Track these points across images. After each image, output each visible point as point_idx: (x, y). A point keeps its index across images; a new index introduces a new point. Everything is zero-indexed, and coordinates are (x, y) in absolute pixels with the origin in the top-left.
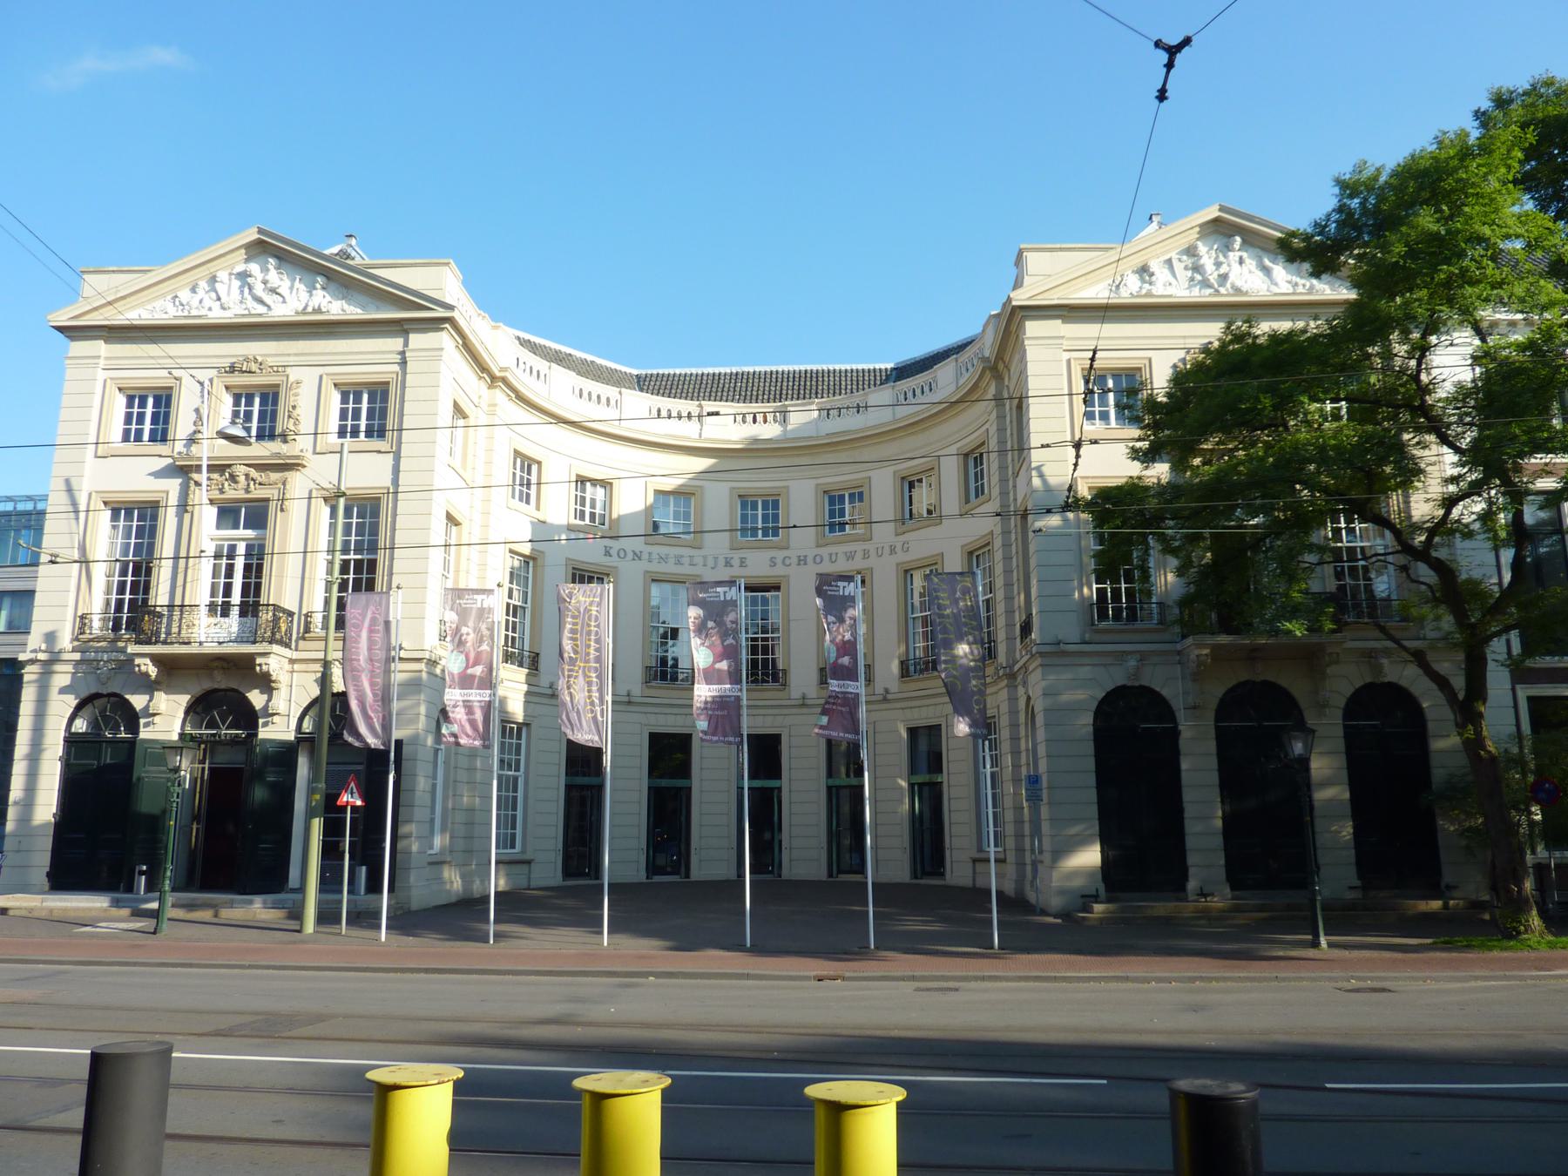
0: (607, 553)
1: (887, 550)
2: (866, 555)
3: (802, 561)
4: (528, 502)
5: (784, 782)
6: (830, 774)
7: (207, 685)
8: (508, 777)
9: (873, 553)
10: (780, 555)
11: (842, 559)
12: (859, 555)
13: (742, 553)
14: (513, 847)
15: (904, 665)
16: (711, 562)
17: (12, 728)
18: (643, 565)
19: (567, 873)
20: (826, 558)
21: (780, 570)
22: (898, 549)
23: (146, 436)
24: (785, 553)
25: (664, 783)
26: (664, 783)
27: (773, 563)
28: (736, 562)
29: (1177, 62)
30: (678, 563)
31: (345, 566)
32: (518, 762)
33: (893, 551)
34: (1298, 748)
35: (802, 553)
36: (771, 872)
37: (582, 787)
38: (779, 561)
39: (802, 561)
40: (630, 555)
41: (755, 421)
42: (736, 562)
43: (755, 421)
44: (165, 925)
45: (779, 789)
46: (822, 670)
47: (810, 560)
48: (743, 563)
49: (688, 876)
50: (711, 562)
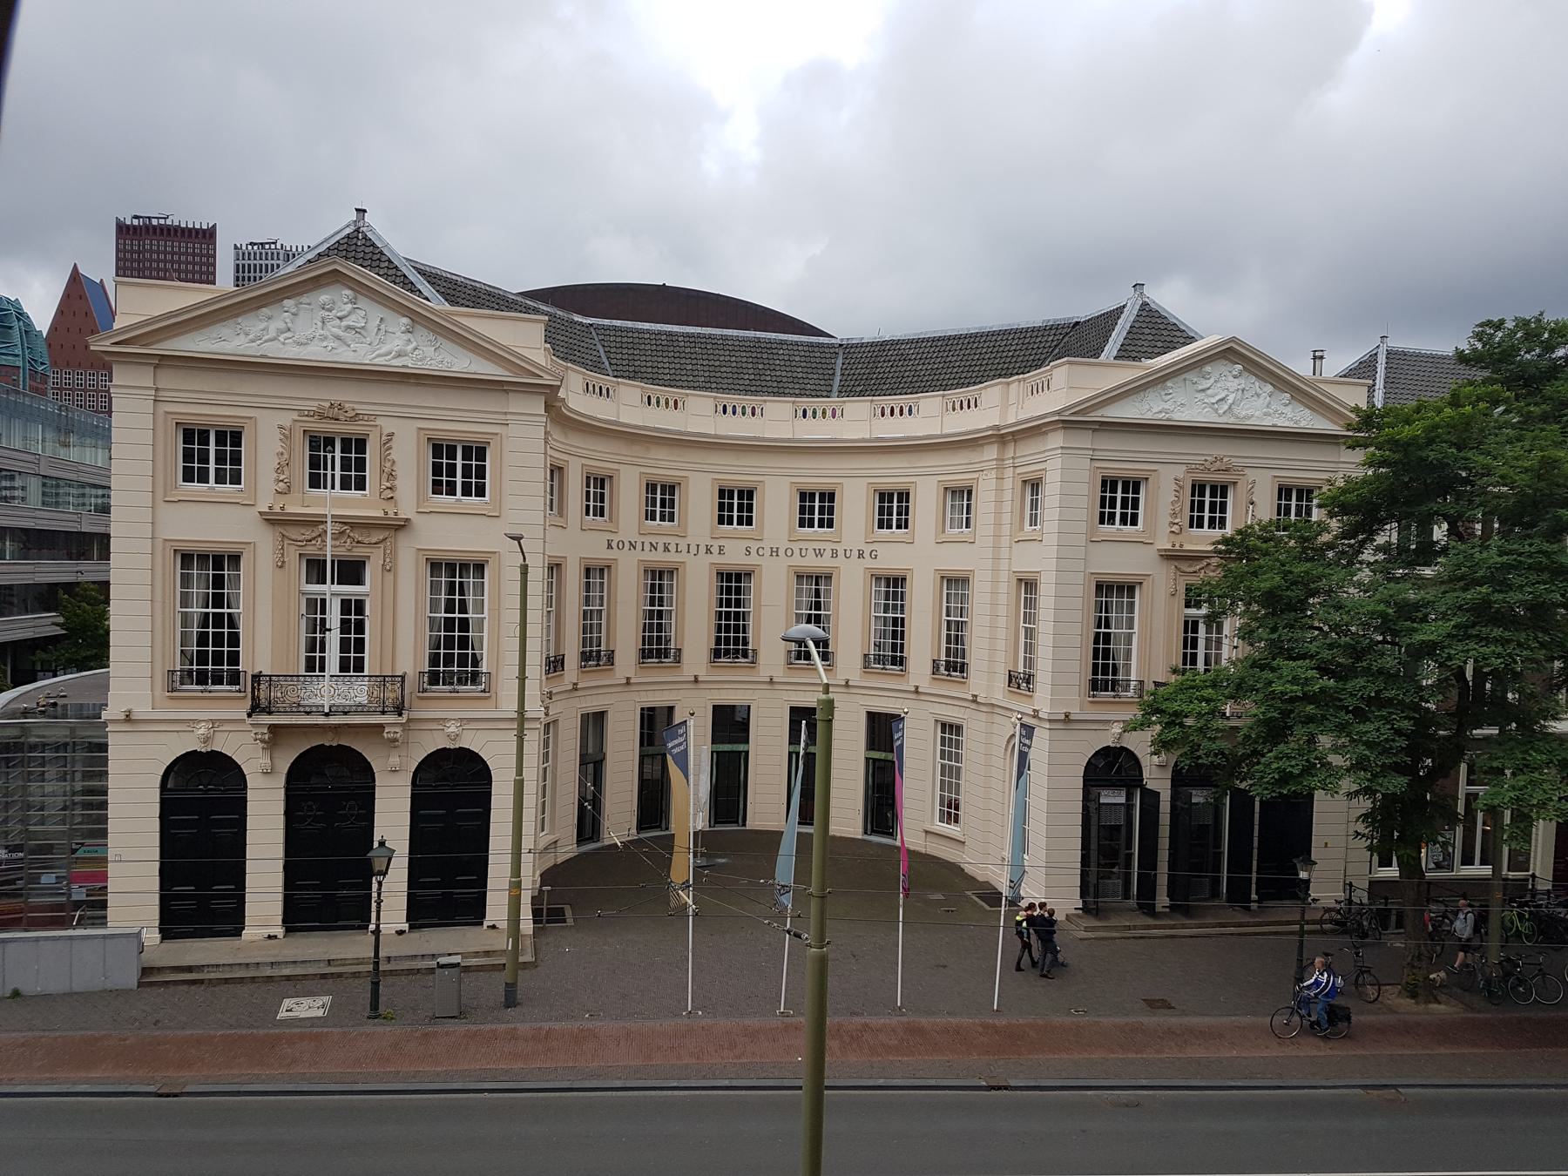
2: (835, 554)
3: (774, 552)
4: (602, 515)
9: (840, 553)
10: (754, 546)
12: (828, 553)
13: (721, 542)
16: (693, 550)
18: (638, 555)
19: (640, 828)
20: (797, 552)
21: (753, 560)
22: (866, 555)
23: (333, 665)
24: (759, 544)
28: (715, 550)
30: (666, 549)
31: (202, 639)
33: (861, 555)
34: (1303, 875)
38: (753, 551)
39: (774, 552)
40: (627, 545)
41: (892, 413)
42: (715, 550)
43: (892, 413)
44: (1298, 917)
45: (747, 753)
47: (781, 552)
50: (693, 550)
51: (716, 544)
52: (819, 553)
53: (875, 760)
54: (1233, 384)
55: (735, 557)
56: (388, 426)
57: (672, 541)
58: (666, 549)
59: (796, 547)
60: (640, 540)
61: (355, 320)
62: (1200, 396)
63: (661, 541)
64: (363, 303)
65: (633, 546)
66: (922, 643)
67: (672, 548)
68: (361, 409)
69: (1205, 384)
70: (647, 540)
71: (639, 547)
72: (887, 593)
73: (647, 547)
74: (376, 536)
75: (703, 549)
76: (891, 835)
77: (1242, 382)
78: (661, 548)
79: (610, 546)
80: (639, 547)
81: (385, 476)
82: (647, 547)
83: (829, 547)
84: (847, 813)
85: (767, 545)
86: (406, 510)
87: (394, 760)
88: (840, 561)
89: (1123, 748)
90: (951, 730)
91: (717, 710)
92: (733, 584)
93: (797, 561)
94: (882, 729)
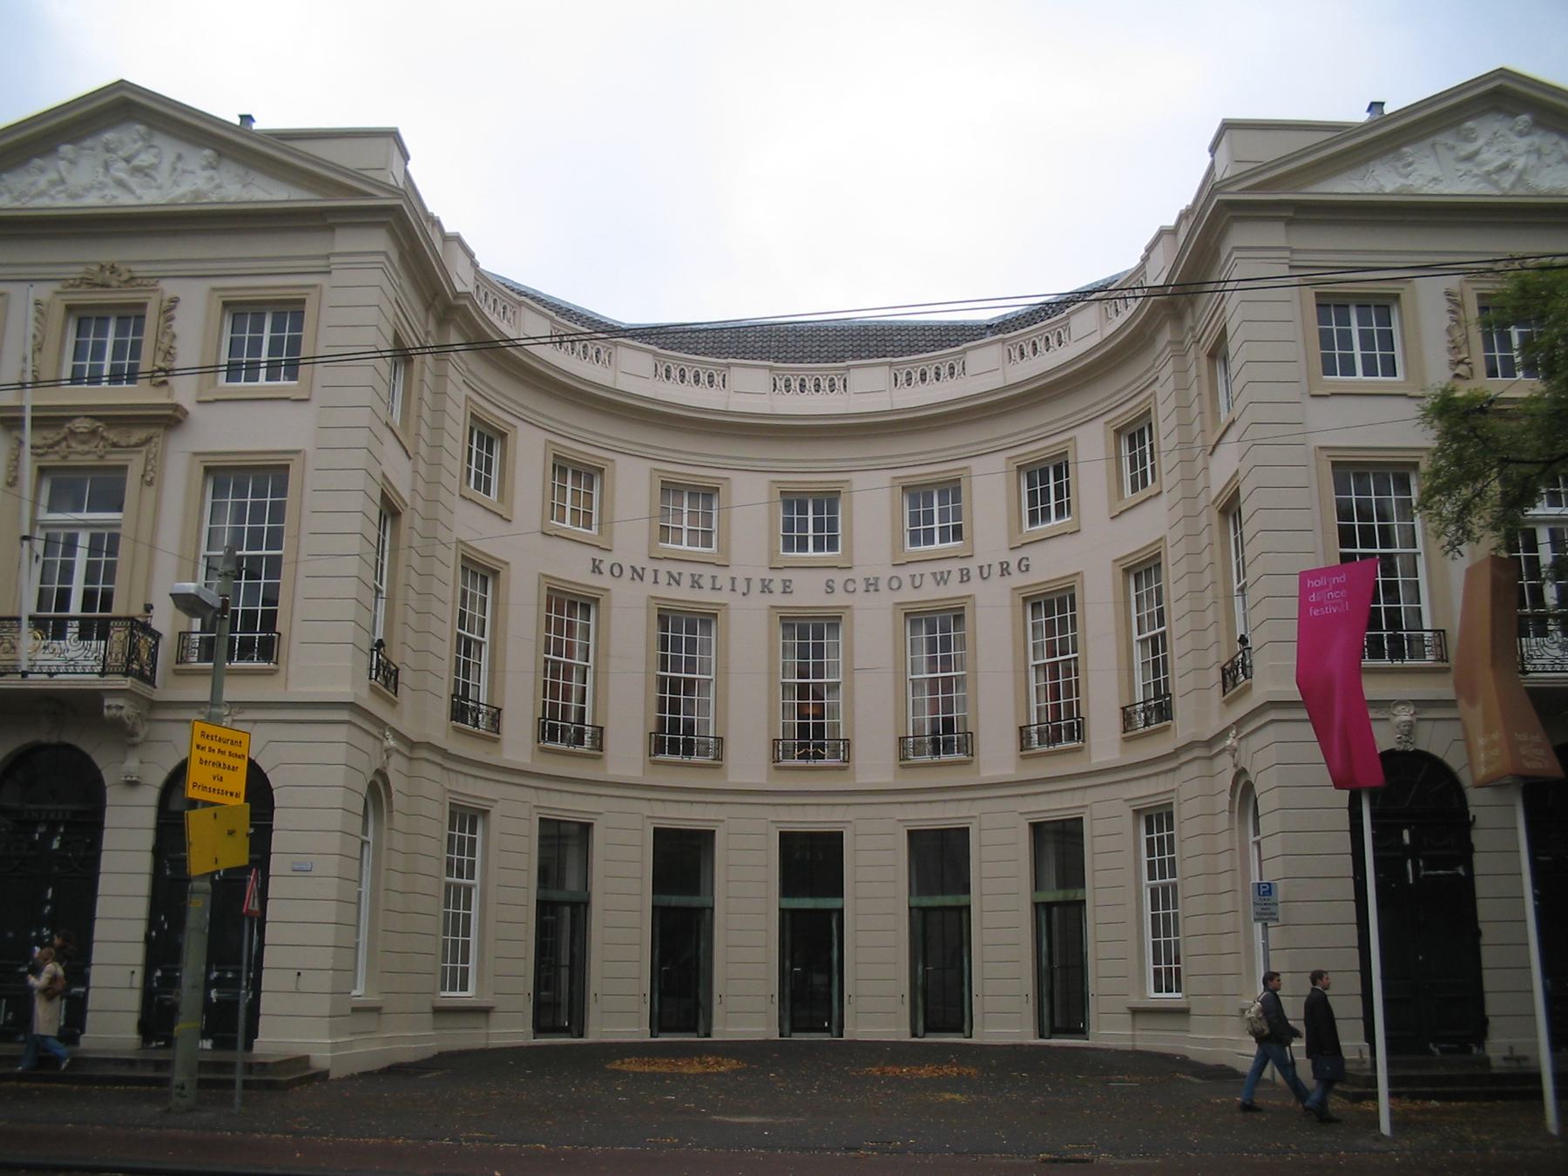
0: (596, 569)
1: (996, 569)
2: (965, 577)
3: (872, 585)
5: (849, 903)
6: (1038, 885)
7: (27, 738)
8: (458, 887)
9: (975, 572)
10: (839, 578)
11: (929, 582)
13: (787, 574)
14: (464, 988)
15: (1023, 731)
16: (741, 586)
17: (1384, 978)
18: (647, 588)
20: (907, 582)
25: (674, 900)
26: (949, 900)
27: (830, 588)
28: (777, 587)
29: (1138, 261)
32: (472, 864)
33: (1005, 570)
35: (871, 575)
36: (828, 1030)
37: (955, 892)
38: (838, 586)
39: (872, 585)
40: (628, 573)
42: (777, 587)
45: (841, 911)
46: (902, 740)
47: (883, 585)
48: (786, 590)
49: (708, 1035)
50: (741, 586)
51: (778, 577)
52: (941, 579)
53: (925, 910)
54: (1522, 144)
55: (809, 593)
56: (170, 288)
57: (707, 572)
58: (696, 583)
59: (904, 573)
60: (651, 566)
61: (145, 159)
62: (1464, 167)
63: (687, 570)
64: (160, 140)
65: (638, 574)
66: (1104, 693)
67: (706, 582)
68: (140, 270)
69: (1470, 148)
70: (664, 567)
71: (649, 576)
72: (1050, 624)
73: (663, 578)
74: (138, 435)
75: (756, 586)
76: (1082, 1033)
77: (1537, 139)
78: (686, 581)
79: (596, 569)
80: (649, 576)
81: (161, 355)
82: (663, 578)
83: (954, 566)
84: (1003, 1009)
85: (858, 574)
86: (183, 392)
87: (132, 764)
88: (975, 587)
89: (1417, 753)
90: (1157, 818)
91: (789, 841)
92: (809, 635)
93: (908, 595)
94: (1059, 845)
